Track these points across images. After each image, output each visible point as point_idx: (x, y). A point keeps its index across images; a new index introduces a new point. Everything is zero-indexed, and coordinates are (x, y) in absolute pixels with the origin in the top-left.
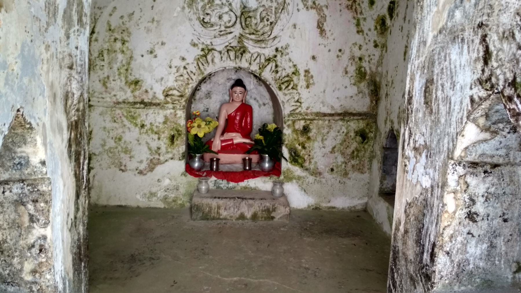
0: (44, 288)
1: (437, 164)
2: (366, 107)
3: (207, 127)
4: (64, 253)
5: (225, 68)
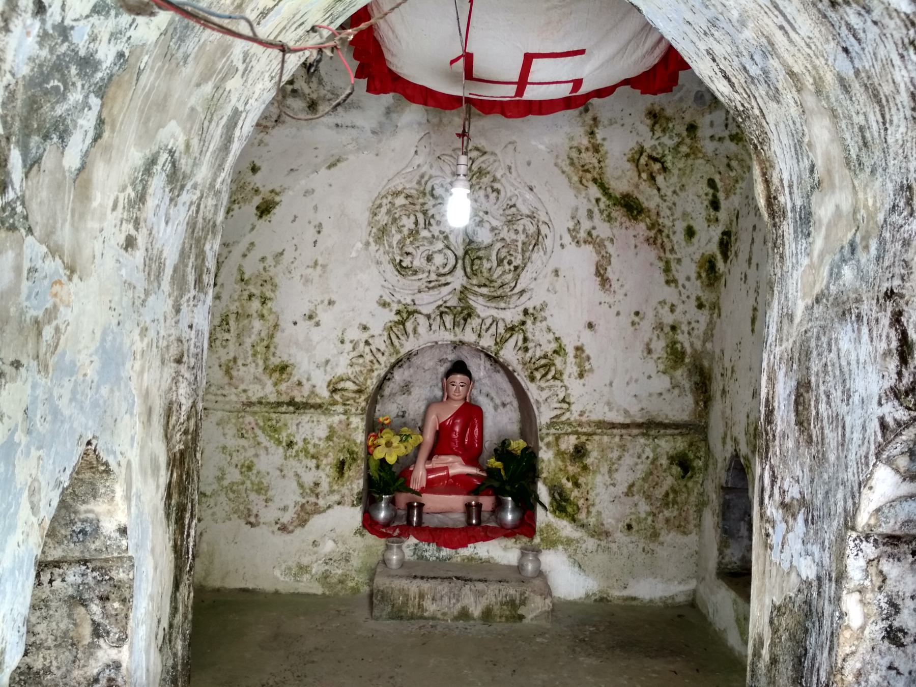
1: (827, 536)
2: (688, 413)
3: (402, 446)
5: (436, 343)
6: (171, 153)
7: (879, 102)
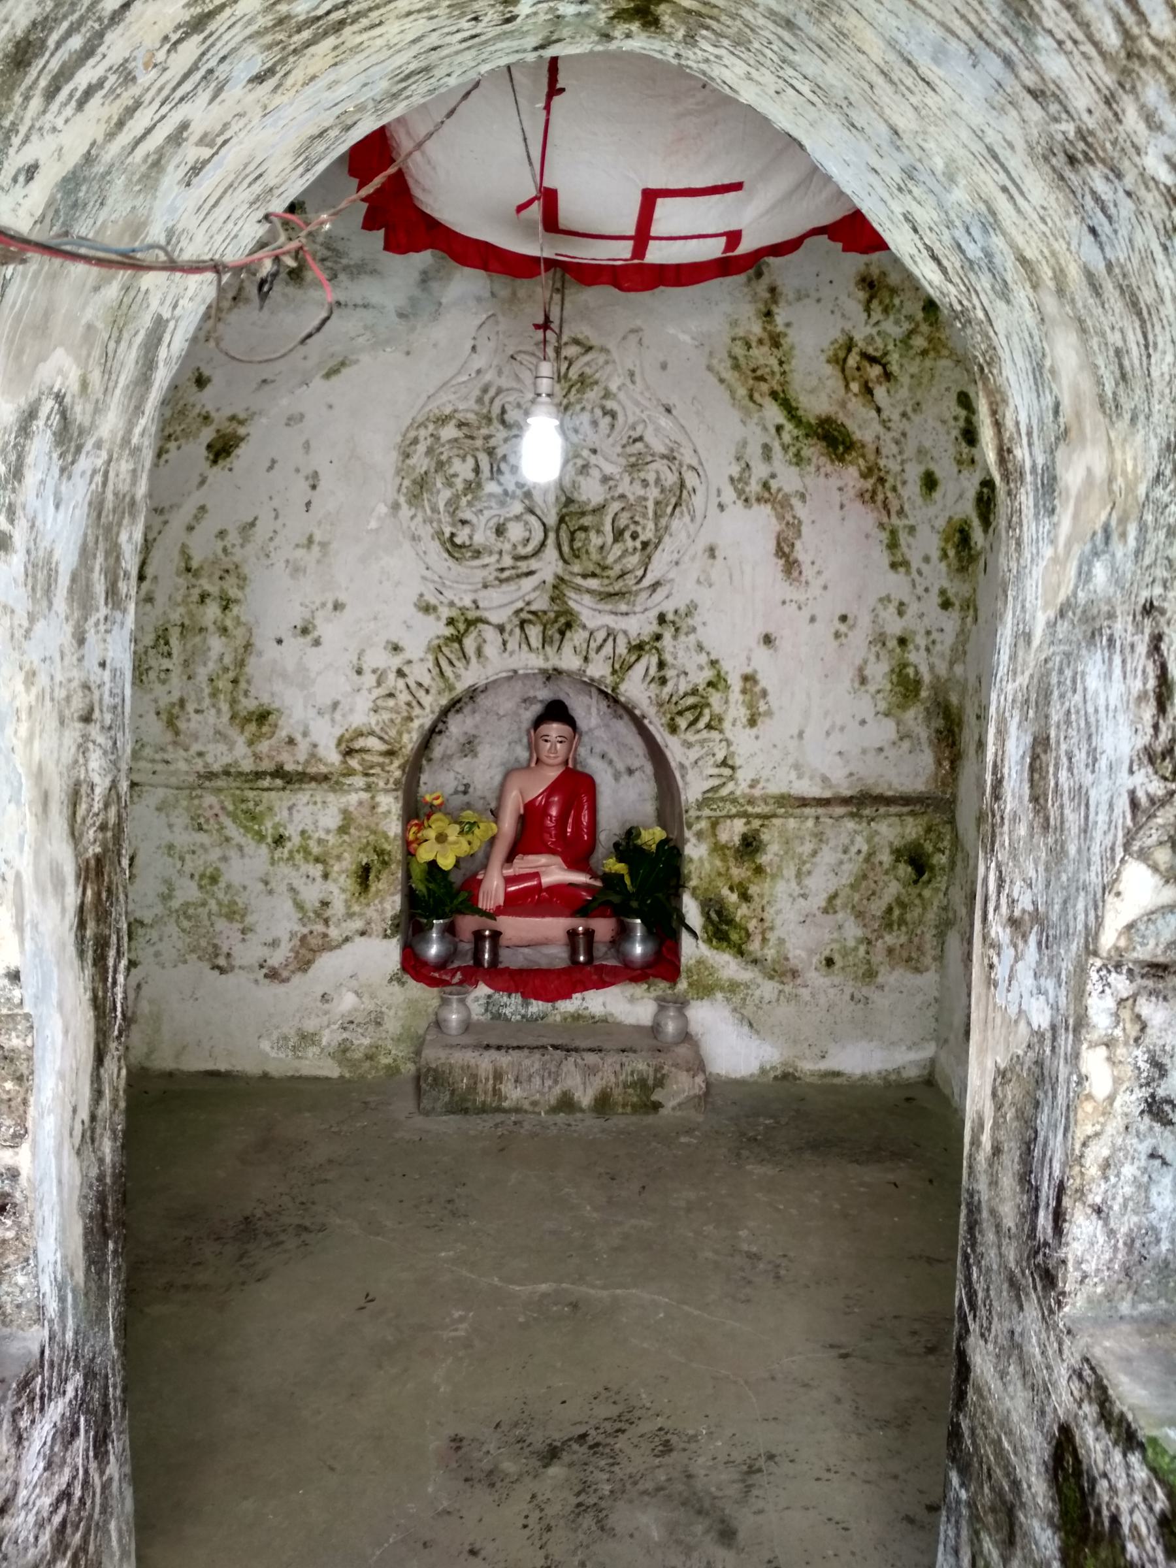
0: (9, 1311)
1: (1064, 965)
2: (924, 779)
3: (463, 841)
4: (62, 1215)
5: (515, 672)
6: (59, 398)
7: (1139, 314)
